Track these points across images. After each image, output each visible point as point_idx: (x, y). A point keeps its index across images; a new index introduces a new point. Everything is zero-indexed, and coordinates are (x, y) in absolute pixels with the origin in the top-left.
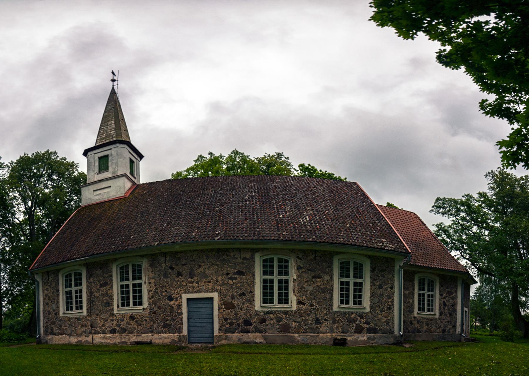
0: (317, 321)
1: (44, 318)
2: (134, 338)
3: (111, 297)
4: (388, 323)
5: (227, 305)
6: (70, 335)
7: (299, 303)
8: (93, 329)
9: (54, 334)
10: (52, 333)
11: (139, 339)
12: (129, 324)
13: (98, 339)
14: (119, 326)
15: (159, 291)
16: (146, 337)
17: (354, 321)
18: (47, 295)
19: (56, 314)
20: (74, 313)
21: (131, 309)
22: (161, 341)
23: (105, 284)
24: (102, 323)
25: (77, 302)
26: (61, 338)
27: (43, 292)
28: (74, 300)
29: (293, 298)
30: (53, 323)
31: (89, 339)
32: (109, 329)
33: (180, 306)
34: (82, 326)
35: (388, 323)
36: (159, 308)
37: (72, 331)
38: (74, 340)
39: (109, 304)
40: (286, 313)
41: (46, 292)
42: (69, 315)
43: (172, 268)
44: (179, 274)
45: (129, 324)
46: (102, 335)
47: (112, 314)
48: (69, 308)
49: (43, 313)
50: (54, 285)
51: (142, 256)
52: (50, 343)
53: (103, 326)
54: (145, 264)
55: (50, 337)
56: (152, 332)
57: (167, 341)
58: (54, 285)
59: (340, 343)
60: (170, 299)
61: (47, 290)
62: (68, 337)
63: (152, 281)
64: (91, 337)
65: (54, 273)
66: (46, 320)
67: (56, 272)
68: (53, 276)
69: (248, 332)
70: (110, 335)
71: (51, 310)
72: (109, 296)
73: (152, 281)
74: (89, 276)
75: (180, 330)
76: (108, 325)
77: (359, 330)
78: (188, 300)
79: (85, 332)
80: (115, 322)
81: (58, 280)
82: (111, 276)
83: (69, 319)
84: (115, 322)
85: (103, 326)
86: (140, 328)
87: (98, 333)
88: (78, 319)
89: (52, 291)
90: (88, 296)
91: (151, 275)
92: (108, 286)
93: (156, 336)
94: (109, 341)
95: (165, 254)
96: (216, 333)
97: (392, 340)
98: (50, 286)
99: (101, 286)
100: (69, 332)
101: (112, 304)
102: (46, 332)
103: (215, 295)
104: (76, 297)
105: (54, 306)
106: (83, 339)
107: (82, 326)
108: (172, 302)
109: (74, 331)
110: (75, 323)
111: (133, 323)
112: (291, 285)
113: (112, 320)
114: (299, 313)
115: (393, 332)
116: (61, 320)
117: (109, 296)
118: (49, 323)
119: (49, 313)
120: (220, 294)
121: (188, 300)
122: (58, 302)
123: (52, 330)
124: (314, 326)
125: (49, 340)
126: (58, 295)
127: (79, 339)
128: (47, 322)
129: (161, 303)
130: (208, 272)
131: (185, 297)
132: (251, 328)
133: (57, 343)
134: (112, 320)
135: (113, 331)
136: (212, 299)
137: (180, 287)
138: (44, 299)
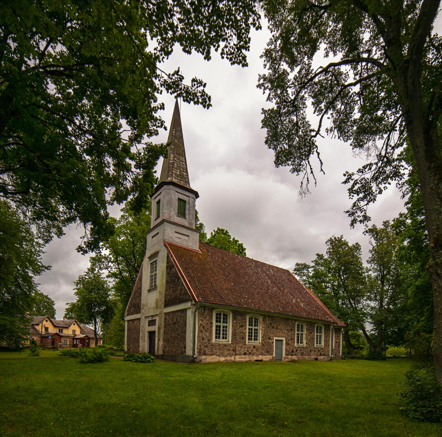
0: (310, 351)
1: (198, 342)
2: (255, 358)
3: (245, 334)
4: (328, 351)
5: (287, 344)
6: (219, 356)
7: (307, 344)
8: (235, 352)
9: (206, 355)
10: (205, 354)
11: (257, 359)
12: (252, 350)
13: (238, 358)
14: (248, 351)
15: (265, 334)
16: (260, 357)
17: (319, 351)
18: (201, 324)
19: (209, 340)
20: (222, 341)
21: (253, 343)
22: (266, 359)
23: (242, 326)
24: (239, 349)
25: (223, 334)
26: (213, 358)
27: (198, 322)
28: (221, 332)
29: (304, 341)
30: (206, 346)
31: (233, 358)
32: (243, 353)
33: (273, 343)
34: (228, 350)
35: (328, 351)
36: (265, 343)
37: (220, 353)
38: (222, 359)
39: (243, 338)
40: (303, 347)
41: (201, 322)
42: (219, 342)
43: (271, 324)
44: (273, 328)
45: (252, 350)
46: (240, 356)
47: (245, 344)
48: (217, 337)
49: (198, 338)
50: (208, 318)
51: (261, 315)
52: (203, 361)
53: (240, 351)
54: (261, 319)
55: (204, 357)
56: (262, 355)
57: (268, 359)
58: (208, 318)
59: (316, 359)
60: (270, 339)
61: (202, 320)
62: (218, 357)
63: (263, 329)
64: (233, 357)
65: (209, 309)
66: (200, 344)
67: (211, 309)
68: (208, 311)
69: (293, 355)
70: (244, 356)
71: (205, 337)
72: (244, 333)
73: (263, 329)
74: (234, 319)
75: (272, 354)
76: (243, 351)
77: (321, 355)
78: (276, 340)
79: (229, 354)
80: (246, 349)
81: (212, 315)
82: (246, 322)
83: (219, 345)
84: (246, 349)
85: (240, 351)
86: (257, 353)
87: (237, 355)
88: (225, 345)
89: (207, 322)
90: (232, 331)
91: (263, 326)
92: (244, 328)
93: (264, 357)
94: (243, 360)
95: (269, 316)
96: (284, 356)
97: (329, 359)
98: (205, 318)
99: (240, 327)
100: (218, 354)
101: (245, 339)
102: (199, 353)
103: (284, 339)
104: (223, 331)
105: (208, 334)
106: (229, 358)
107: (228, 350)
108: (270, 341)
109: (222, 353)
110: (223, 348)
111: (254, 350)
112: (304, 336)
113: (245, 348)
114: (306, 348)
115: (329, 355)
116: (213, 345)
117: (244, 333)
118: (203, 346)
119: (203, 339)
120: (286, 339)
121: (276, 340)
122: (211, 331)
123: (205, 351)
124: (310, 353)
125: (204, 359)
126: (211, 327)
127: (227, 358)
128: (200, 346)
129: (266, 341)
130: (282, 328)
131: (275, 338)
132: (294, 354)
133: (209, 361)
134: (245, 348)
135: (245, 354)
136: (282, 340)
137: (273, 334)
138: (199, 327)
